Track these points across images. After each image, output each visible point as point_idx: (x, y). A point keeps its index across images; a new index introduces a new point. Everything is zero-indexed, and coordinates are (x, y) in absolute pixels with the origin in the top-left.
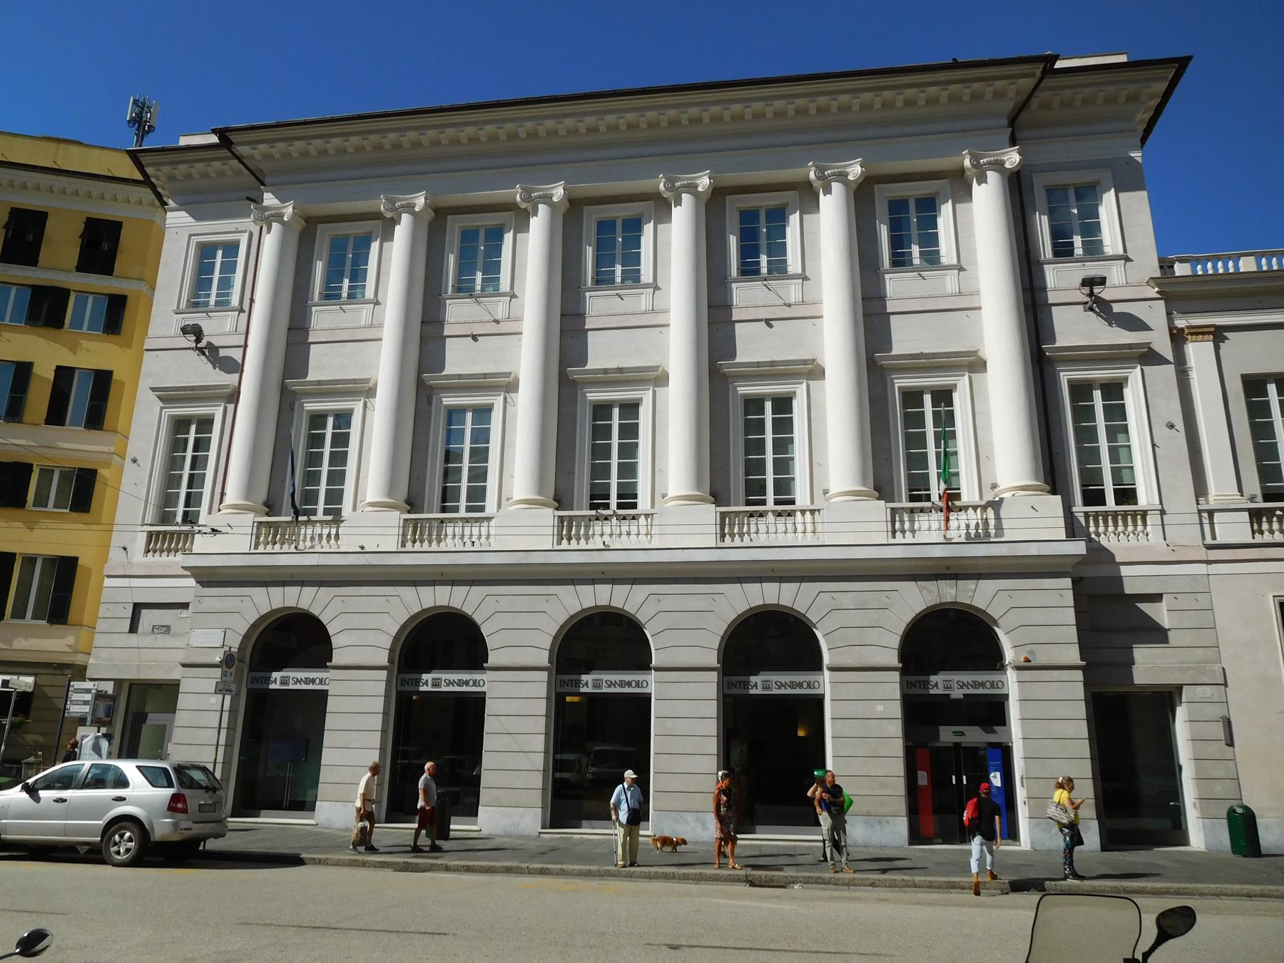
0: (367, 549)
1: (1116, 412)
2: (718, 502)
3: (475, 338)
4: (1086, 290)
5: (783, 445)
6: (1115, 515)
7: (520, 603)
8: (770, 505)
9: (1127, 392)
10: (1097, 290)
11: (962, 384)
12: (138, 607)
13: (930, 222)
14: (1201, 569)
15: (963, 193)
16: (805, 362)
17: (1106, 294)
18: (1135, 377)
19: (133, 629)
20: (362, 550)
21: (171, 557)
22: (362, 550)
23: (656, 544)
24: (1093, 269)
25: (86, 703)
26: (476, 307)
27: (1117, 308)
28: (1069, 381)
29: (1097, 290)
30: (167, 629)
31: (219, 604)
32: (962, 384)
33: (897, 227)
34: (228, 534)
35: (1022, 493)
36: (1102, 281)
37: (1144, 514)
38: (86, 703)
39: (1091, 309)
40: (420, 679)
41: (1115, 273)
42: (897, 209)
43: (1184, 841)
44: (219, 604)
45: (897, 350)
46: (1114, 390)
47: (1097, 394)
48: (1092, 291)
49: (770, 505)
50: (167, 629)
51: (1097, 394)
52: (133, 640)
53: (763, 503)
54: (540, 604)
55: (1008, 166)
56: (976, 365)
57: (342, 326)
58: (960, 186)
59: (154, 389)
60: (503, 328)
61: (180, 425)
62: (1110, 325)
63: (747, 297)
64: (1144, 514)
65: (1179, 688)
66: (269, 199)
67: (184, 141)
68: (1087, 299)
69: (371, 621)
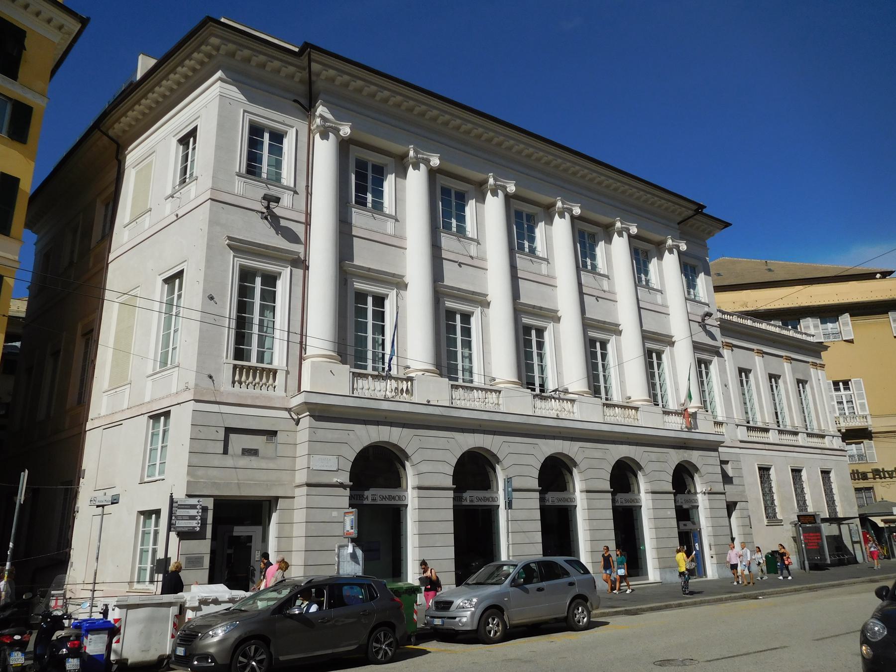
0: (431, 403)
1: (269, 296)
2: (451, 379)
3: (460, 264)
4: (265, 203)
5: (541, 357)
6: (255, 369)
7: (522, 448)
8: (370, 370)
9: (279, 283)
10: (273, 205)
11: (392, 294)
12: (229, 431)
13: (461, 208)
14: (737, 451)
15: (402, 173)
16: (394, 275)
17: (278, 211)
18: (286, 272)
19: (225, 452)
20: (428, 404)
21: (257, 391)
22: (428, 404)
23: (640, 424)
24: (274, 191)
25: (192, 518)
26: (457, 242)
27: (283, 223)
28: (240, 265)
29: (273, 205)
30: (253, 452)
31: (330, 436)
32: (392, 294)
33: (361, 177)
34: (324, 376)
35: (427, 374)
36: (277, 200)
37: (275, 372)
38: (192, 518)
39: (266, 218)
40: (363, 496)
41: (286, 199)
42: (361, 167)
43: (705, 574)
44: (330, 436)
45: (357, 262)
46: (270, 280)
47: (258, 280)
48: (269, 205)
49: (370, 370)
50: (253, 452)
51: (258, 280)
52: (228, 461)
53: (365, 368)
54: (442, 443)
55: (341, 133)
56: (400, 284)
57: (375, 229)
58: (401, 167)
59: (229, 238)
60: (475, 262)
61: (246, 275)
62: (277, 234)
63: (359, 218)
64: (275, 372)
65: (277, 498)
66: (321, 110)
67: (223, 20)
68: (265, 210)
69: (439, 455)
